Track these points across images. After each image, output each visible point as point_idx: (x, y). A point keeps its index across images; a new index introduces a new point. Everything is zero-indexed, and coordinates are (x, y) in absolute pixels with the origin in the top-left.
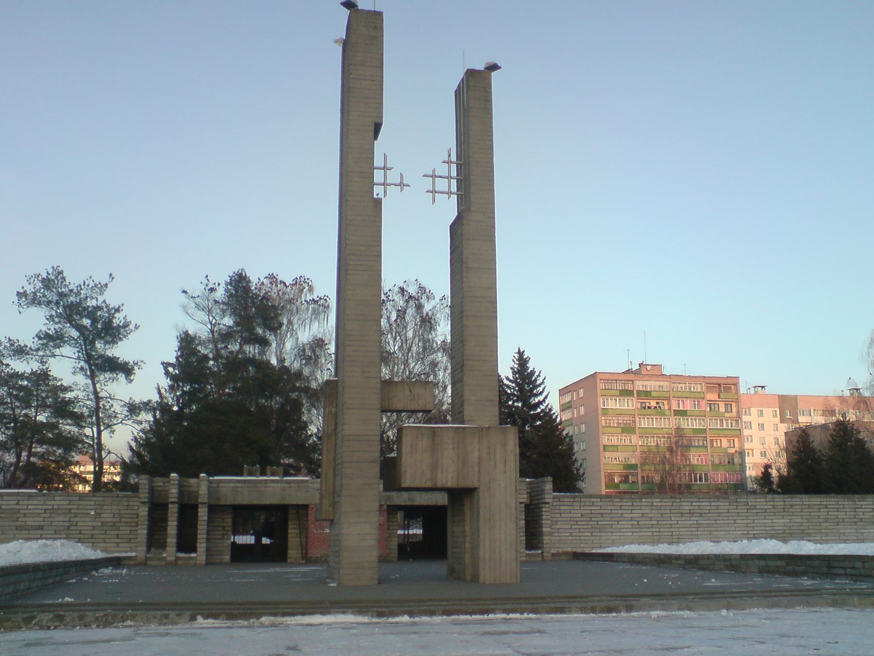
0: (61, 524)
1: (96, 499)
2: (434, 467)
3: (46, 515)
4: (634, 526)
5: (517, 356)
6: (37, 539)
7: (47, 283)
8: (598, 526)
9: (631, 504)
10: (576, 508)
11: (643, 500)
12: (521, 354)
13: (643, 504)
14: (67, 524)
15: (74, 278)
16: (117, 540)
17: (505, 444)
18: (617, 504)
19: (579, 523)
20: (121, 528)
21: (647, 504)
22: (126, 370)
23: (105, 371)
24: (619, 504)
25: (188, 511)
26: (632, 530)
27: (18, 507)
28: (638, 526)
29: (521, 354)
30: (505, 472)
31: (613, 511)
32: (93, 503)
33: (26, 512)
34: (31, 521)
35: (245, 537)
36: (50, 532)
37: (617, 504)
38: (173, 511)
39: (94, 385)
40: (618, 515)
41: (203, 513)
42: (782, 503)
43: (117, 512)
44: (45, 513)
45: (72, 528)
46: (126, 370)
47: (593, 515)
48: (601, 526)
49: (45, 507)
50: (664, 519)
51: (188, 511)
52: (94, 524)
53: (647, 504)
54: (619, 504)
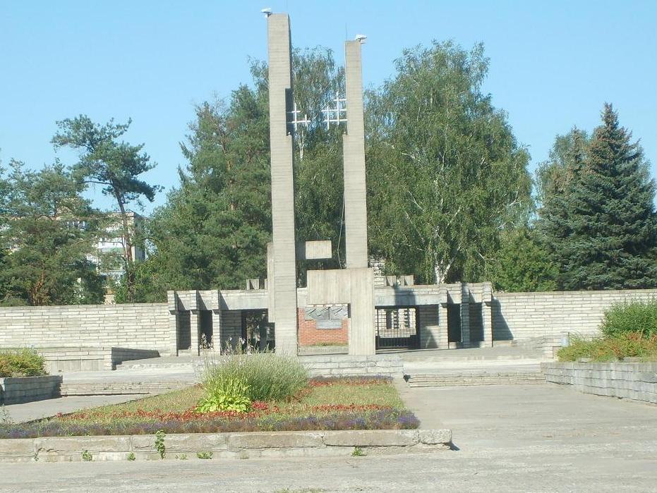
0: (112, 328)
1: (136, 308)
2: (326, 293)
3: (101, 322)
4: (584, 318)
5: (604, 110)
6: (600, 286)
7: (77, 126)
8: (551, 319)
9: (581, 299)
10: (530, 304)
11: (593, 296)
12: (609, 108)
13: (593, 299)
14: (117, 328)
15: (99, 121)
16: (155, 339)
17: (366, 279)
18: (568, 300)
19: (533, 316)
20: (157, 330)
21: (597, 299)
22: (149, 192)
23: (129, 191)
24: (571, 299)
25: (205, 317)
26: (581, 322)
27: (79, 316)
28: (587, 318)
29: (609, 108)
30: (366, 294)
31: (564, 306)
32: (134, 311)
33: (86, 319)
34: (90, 327)
35: (485, 333)
36: (105, 334)
37: (568, 300)
38: (194, 321)
39: (121, 205)
40: (569, 309)
41: (216, 319)
42: (647, 298)
43: (153, 317)
44: (99, 320)
45: (120, 331)
46: (149, 192)
47: (546, 310)
48: (534, 319)
49: (99, 316)
50: (556, 312)
51: (205, 317)
52: (137, 327)
53: (597, 299)
54: (571, 299)
